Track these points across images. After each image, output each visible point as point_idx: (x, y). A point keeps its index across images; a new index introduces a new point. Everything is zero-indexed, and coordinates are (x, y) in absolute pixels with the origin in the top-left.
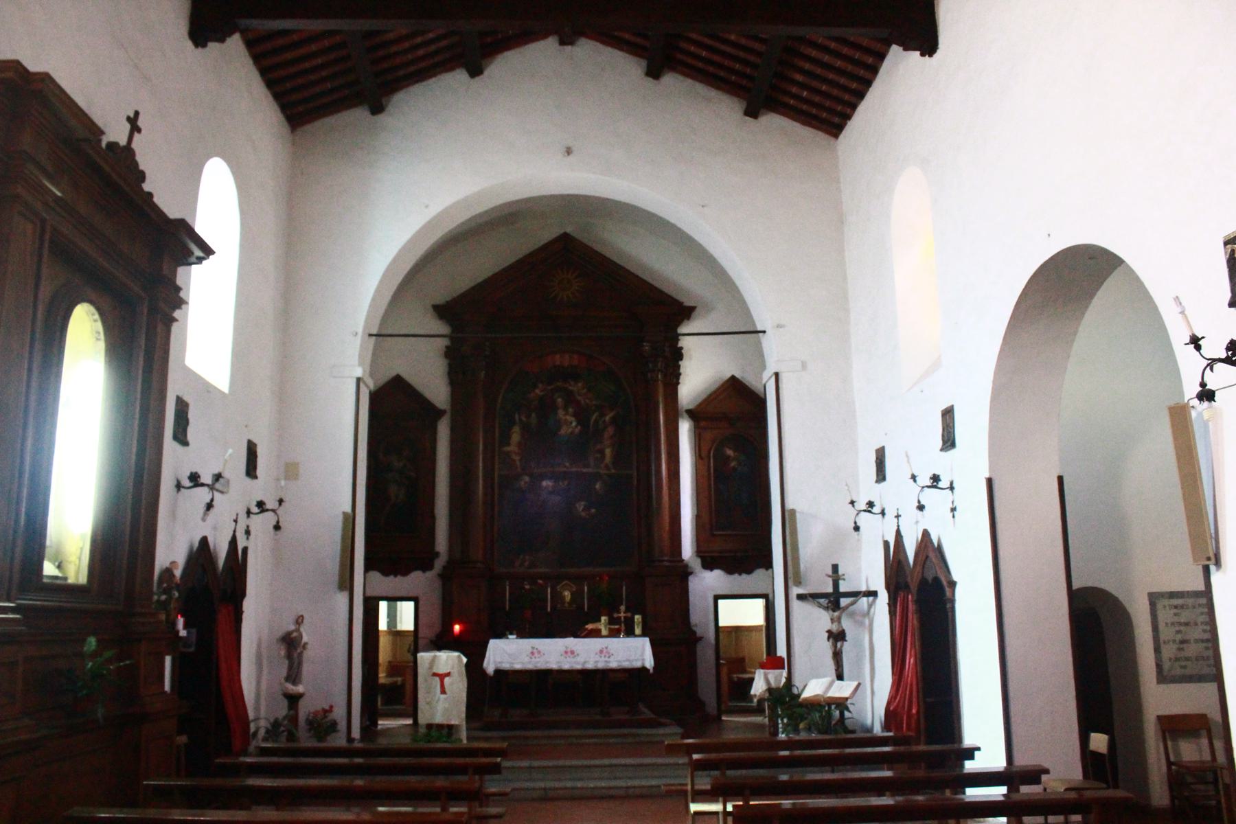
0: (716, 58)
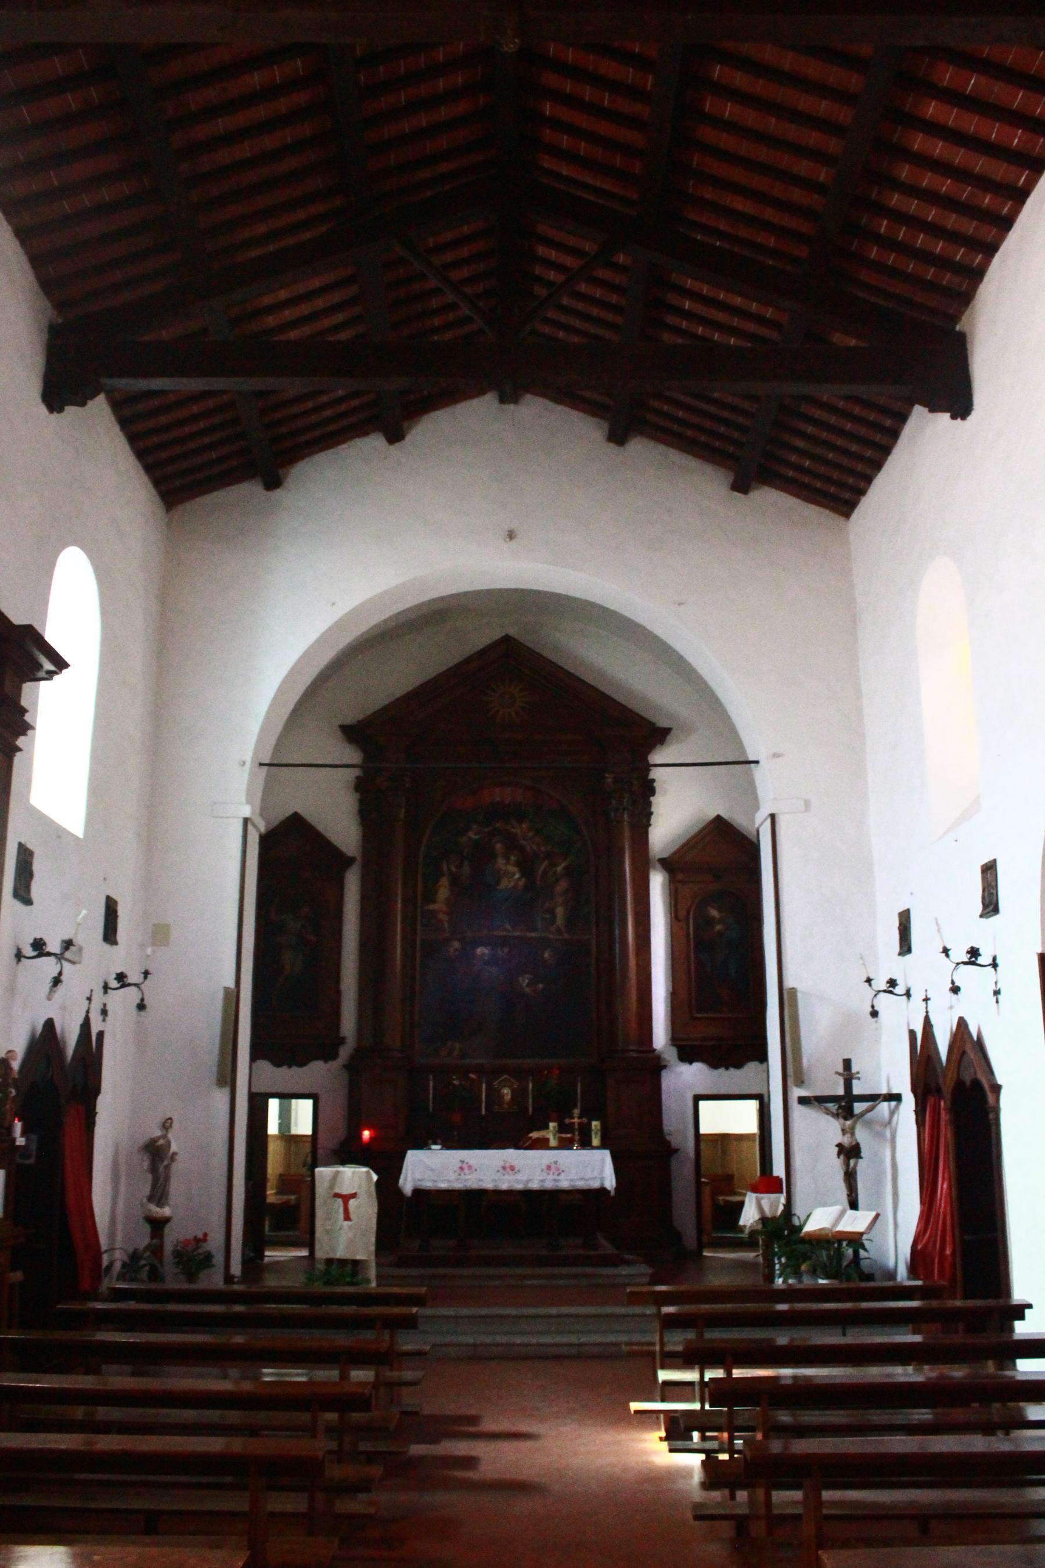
0: (695, 420)
